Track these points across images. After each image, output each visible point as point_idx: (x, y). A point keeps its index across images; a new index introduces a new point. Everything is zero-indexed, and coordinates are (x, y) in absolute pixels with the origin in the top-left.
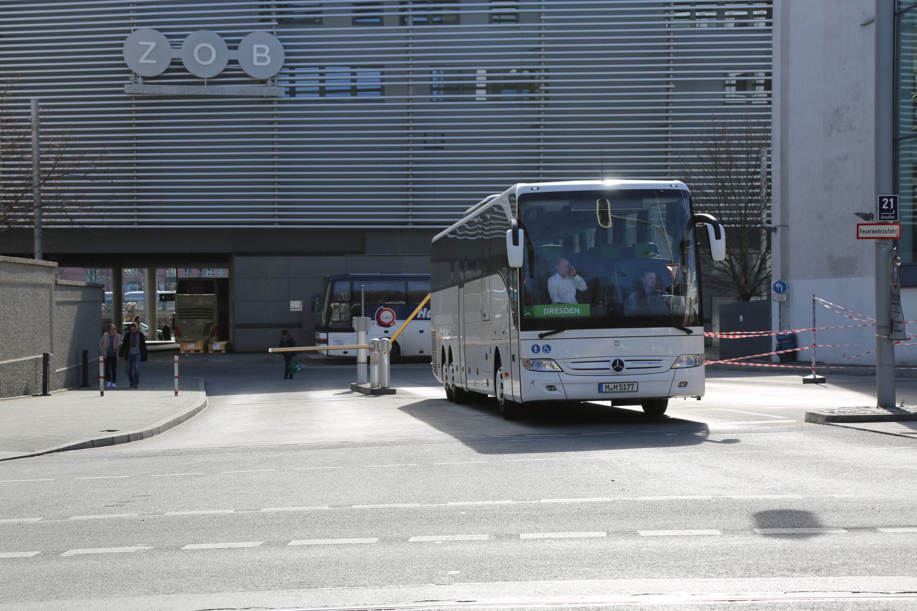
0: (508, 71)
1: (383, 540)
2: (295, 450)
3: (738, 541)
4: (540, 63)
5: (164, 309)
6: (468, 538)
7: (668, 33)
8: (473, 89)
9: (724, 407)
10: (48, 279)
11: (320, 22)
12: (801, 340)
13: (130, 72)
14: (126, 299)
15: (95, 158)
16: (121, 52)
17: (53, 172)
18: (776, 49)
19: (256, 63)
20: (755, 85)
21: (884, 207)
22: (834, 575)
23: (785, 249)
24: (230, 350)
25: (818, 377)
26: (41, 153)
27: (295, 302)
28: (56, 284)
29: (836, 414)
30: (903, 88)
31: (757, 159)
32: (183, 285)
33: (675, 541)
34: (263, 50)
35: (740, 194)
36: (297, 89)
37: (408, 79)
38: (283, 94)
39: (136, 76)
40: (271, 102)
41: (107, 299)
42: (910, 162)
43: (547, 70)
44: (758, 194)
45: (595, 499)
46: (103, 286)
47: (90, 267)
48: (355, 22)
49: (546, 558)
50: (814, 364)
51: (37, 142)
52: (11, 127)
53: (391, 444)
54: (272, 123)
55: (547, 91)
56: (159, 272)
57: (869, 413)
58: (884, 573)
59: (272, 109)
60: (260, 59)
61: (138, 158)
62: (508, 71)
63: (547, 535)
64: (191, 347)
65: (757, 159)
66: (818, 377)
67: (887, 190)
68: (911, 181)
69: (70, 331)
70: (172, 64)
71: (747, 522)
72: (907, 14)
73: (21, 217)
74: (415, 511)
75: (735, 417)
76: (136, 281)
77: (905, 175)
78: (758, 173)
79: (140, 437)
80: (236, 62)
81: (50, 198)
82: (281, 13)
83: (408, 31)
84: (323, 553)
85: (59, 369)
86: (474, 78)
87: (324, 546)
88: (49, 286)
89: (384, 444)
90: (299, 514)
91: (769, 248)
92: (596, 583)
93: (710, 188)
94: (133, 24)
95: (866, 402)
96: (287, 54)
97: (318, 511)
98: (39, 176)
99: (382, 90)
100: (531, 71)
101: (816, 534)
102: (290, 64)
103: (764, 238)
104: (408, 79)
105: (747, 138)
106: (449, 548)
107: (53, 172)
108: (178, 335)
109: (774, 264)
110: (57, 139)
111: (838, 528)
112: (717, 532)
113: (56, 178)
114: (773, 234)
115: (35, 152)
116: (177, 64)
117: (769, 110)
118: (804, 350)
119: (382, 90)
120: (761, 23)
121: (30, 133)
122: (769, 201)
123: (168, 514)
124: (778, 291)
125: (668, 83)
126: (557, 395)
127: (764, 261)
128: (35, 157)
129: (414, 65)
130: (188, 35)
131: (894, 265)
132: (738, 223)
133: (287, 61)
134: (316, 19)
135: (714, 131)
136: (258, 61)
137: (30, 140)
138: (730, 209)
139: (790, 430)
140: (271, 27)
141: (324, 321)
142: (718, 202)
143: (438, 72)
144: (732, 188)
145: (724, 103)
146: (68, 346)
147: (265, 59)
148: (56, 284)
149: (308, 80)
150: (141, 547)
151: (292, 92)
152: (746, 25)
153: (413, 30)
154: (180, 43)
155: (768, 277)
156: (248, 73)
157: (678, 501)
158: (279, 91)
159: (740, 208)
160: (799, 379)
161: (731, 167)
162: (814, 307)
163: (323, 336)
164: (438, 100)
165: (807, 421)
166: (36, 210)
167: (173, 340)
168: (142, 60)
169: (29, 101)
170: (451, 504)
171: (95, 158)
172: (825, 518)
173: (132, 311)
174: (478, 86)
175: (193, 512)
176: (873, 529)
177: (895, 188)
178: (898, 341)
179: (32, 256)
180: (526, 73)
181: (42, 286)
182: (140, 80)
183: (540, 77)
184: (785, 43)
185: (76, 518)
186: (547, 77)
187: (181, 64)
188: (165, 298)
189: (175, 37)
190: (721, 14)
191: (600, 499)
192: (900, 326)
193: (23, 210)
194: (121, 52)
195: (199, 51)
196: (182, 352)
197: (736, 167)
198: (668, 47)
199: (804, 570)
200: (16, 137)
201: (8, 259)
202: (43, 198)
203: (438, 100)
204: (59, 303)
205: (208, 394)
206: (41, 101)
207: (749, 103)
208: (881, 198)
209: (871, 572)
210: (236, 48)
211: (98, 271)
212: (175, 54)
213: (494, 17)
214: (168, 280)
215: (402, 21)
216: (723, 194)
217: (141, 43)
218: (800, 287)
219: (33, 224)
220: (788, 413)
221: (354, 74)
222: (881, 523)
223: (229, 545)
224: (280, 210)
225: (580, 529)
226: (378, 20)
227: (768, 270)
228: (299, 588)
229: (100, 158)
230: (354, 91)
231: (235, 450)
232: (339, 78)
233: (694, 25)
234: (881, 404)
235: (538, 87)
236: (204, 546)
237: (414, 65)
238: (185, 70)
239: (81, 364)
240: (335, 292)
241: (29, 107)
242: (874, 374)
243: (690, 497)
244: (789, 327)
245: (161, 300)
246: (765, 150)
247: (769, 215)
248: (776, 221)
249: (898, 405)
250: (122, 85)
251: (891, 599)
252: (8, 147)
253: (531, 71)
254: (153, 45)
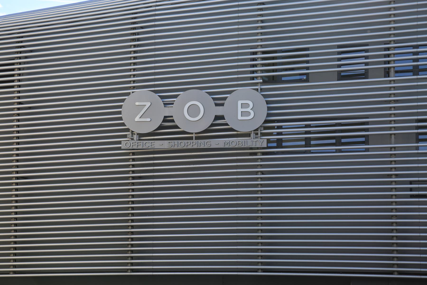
13: (128, 130)
19: (240, 118)
34: (247, 105)
37: (390, 129)
70: (164, 121)
80: (222, 118)
96: (269, 109)
104: (390, 129)
133: (269, 115)
140: (256, 84)
147: (248, 114)
168: (137, 119)
187: (173, 121)
194: (120, 113)
210: (222, 105)
212: (167, 112)
238: (176, 127)
250: (120, 143)
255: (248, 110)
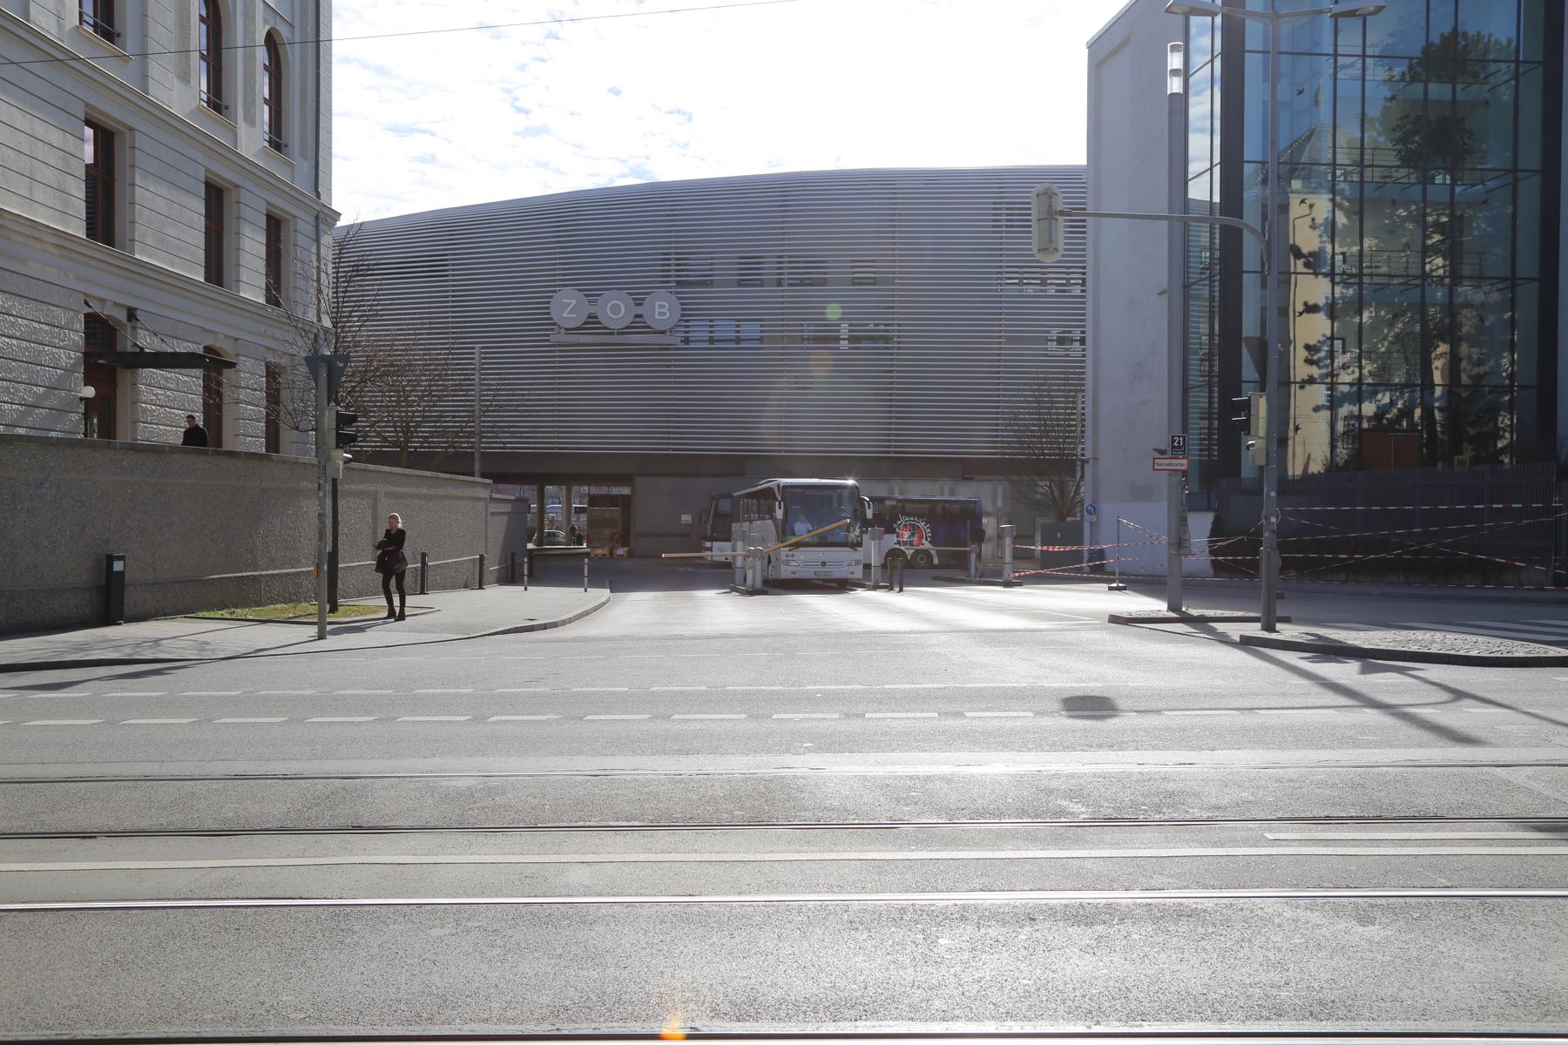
0: (867, 325)
1: (751, 716)
2: (681, 639)
3: (1047, 722)
4: (893, 319)
5: (578, 520)
6: (822, 716)
7: (1001, 296)
8: (837, 339)
9: (1042, 610)
10: (485, 493)
11: (711, 284)
12: (1107, 553)
13: (555, 324)
14: (548, 511)
15: (524, 395)
16: (548, 308)
17: (491, 406)
18: (1089, 311)
19: (657, 317)
20: (1072, 340)
21: (1175, 444)
22: (1124, 750)
23: (1095, 478)
24: (631, 554)
25: (1120, 585)
26: (482, 390)
27: (686, 516)
28: (491, 498)
29: (1134, 616)
30: (1191, 346)
31: (1073, 402)
32: (594, 500)
33: (995, 722)
34: (664, 307)
35: (1059, 432)
36: (691, 339)
37: (783, 331)
38: (679, 343)
39: (560, 327)
40: (669, 349)
41: (532, 510)
42: (1198, 407)
43: (899, 325)
44: (1074, 432)
45: (930, 686)
46: (528, 500)
47: (520, 484)
48: (740, 283)
49: (885, 734)
50: (1117, 574)
51: (479, 382)
52: (459, 369)
53: (761, 636)
54: (669, 366)
55: (899, 343)
56: (575, 488)
57: (1160, 615)
58: (1165, 748)
59: (670, 355)
60: (660, 314)
61: (559, 438)
62: (867, 325)
63: (889, 715)
64: (599, 551)
65: (1073, 402)
66: (1120, 585)
67: (1178, 430)
68: (1198, 424)
69: (501, 536)
70: (589, 317)
71: (1056, 706)
72: (1194, 287)
73: (465, 442)
74: (778, 692)
75: (1051, 618)
76: (556, 498)
77: (1193, 418)
78: (1074, 414)
79: (554, 625)
80: (641, 316)
81: (488, 427)
82: (679, 276)
83: (783, 291)
84: (699, 726)
85: (493, 567)
86: (839, 331)
87: (701, 720)
88: (486, 499)
89: (756, 636)
90: (682, 693)
91: (1082, 476)
92: (927, 755)
93: (1034, 425)
94: (559, 285)
95: (1158, 606)
96: (683, 310)
97: (698, 691)
98: (479, 409)
99: (761, 340)
100: (886, 325)
101: (1114, 716)
102: (685, 317)
103: (1079, 468)
104: (783, 331)
105: (1065, 385)
106: (805, 725)
107: (491, 406)
108: (589, 542)
109: (1086, 489)
110: (495, 379)
111: (1131, 711)
112: (1031, 714)
113: (493, 411)
114: (1086, 465)
115: (478, 390)
116: (593, 318)
117: (1084, 361)
118: (1109, 561)
119: (761, 340)
120: (1077, 291)
121: (473, 374)
122: (1083, 437)
123: (574, 690)
124: (1089, 513)
125: (1000, 337)
126: (797, 576)
127: (1078, 487)
128: (478, 393)
129: (788, 320)
130: (602, 294)
131: (1182, 492)
132: (1057, 455)
133: (682, 315)
134: (707, 280)
135: (1038, 378)
136: (659, 315)
137: (473, 380)
138: (1051, 443)
139: (1096, 629)
140: (671, 287)
141: (709, 532)
142: (1041, 437)
143: (809, 325)
144: (1053, 426)
145: (1047, 355)
146: (500, 549)
147: (664, 314)
148: (491, 498)
149: (699, 331)
150: (551, 716)
151: (686, 341)
152: (1064, 291)
153: (788, 291)
154: (596, 301)
155: (1082, 501)
156: (651, 325)
157: (999, 688)
158: (676, 340)
159: (1059, 443)
160: (1105, 586)
161: (1051, 408)
162: (1118, 527)
163: (708, 544)
164: (808, 348)
165: (1109, 622)
166: (477, 437)
167: (585, 545)
168: (565, 315)
169: (473, 348)
170: (809, 687)
171: (524, 395)
172: (1121, 703)
173: (552, 521)
174: (841, 337)
175: (595, 689)
176: (1158, 712)
177: (1185, 428)
178: (1186, 555)
179: (473, 475)
180: (883, 327)
181: (479, 499)
182: (562, 331)
183: (893, 331)
184: (1096, 308)
185: (499, 690)
186: (899, 331)
187: (596, 317)
188: (579, 511)
189: (592, 295)
190: (1044, 282)
191: (935, 686)
192: (1187, 544)
193: (466, 437)
194: (548, 308)
195: (617, 304)
196: (592, 556)
197: (1056, 408)
198: (1001, 308)
199: (1100, 746)
200: (463, 377)
201: (453, 476)
202: (483, 427)
203: (808, 348)
204: (493, 514)
205: (611, 592)
206: (483, 348)
207: (1067, 356)
208: (1173, 437)
209: (1155, 748)
210: (641, 305)
211: (526, 487)
212: (592, 310)
213: (856, 281)
214: (582, 496)
215: (779, 283)
216: (1045, 431)
217: (564, 301)
218: (1107, 509)
219: (474, 448)
220: (1094, 615)
221: (738, 326)
222: (1164, 707)
223: (623, 717)
224: (674, 438)
225: (916, 710)
226: (759, 282)
227: (1082, 495)
228: (678, 754)
229: (529, 395)
230: (738, 340)
231: (632, 638)
232: (726, 329)
233: (1021, 291)
234: (1170, 609)
235: (892, 339)
236: (602, 717)
237: (788, 320)
238: (600, 323)
239: (510, 563)
240: (719, 508)
241: (473, 353)
242: (1166, 584)
243: (1010, 685)
244: (1098, 544)
245: (576, 512)
246: (1080, 395)
247: (1083, 449)
248: (1089, 454)
249: (1184, 609)
250: (548, 335)
251: (1169, 770)
252: (457, 385)
253: (886, 325)
254: (574, 302)
255: (664, 310)
